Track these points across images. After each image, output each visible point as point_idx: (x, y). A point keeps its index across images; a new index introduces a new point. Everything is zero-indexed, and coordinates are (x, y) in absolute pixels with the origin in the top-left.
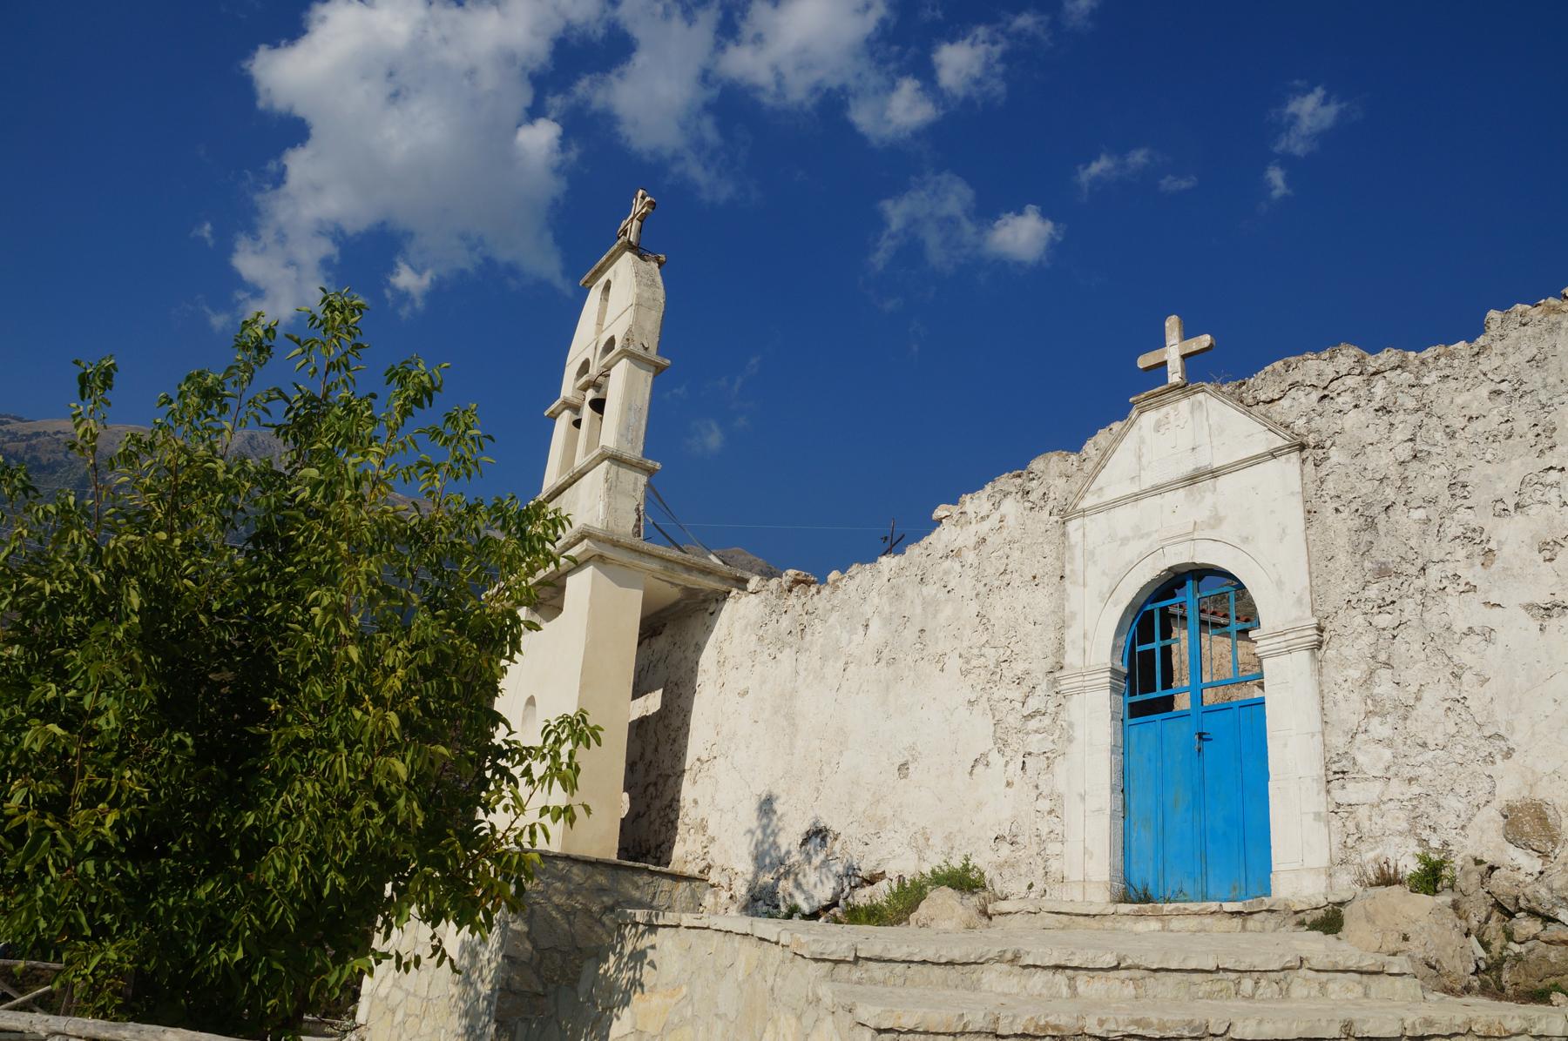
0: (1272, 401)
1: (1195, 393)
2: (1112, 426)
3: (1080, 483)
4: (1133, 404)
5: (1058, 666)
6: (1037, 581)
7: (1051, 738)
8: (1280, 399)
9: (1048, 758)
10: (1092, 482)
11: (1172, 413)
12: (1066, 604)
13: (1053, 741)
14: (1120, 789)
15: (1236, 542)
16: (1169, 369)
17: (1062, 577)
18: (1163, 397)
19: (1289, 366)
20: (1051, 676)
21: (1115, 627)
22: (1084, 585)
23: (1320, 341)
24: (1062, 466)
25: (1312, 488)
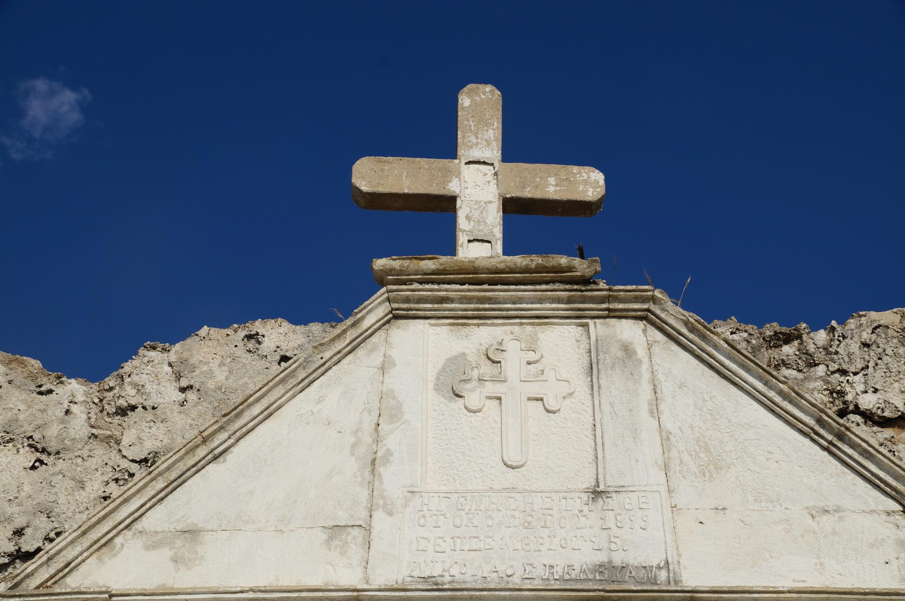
1: (612, 314)
2: (258, 326)
3: (95, 487)
4: (380, 281)
10: (160, 498)
16: (462, 223)
18: (500, 292)
23: (470, 83)
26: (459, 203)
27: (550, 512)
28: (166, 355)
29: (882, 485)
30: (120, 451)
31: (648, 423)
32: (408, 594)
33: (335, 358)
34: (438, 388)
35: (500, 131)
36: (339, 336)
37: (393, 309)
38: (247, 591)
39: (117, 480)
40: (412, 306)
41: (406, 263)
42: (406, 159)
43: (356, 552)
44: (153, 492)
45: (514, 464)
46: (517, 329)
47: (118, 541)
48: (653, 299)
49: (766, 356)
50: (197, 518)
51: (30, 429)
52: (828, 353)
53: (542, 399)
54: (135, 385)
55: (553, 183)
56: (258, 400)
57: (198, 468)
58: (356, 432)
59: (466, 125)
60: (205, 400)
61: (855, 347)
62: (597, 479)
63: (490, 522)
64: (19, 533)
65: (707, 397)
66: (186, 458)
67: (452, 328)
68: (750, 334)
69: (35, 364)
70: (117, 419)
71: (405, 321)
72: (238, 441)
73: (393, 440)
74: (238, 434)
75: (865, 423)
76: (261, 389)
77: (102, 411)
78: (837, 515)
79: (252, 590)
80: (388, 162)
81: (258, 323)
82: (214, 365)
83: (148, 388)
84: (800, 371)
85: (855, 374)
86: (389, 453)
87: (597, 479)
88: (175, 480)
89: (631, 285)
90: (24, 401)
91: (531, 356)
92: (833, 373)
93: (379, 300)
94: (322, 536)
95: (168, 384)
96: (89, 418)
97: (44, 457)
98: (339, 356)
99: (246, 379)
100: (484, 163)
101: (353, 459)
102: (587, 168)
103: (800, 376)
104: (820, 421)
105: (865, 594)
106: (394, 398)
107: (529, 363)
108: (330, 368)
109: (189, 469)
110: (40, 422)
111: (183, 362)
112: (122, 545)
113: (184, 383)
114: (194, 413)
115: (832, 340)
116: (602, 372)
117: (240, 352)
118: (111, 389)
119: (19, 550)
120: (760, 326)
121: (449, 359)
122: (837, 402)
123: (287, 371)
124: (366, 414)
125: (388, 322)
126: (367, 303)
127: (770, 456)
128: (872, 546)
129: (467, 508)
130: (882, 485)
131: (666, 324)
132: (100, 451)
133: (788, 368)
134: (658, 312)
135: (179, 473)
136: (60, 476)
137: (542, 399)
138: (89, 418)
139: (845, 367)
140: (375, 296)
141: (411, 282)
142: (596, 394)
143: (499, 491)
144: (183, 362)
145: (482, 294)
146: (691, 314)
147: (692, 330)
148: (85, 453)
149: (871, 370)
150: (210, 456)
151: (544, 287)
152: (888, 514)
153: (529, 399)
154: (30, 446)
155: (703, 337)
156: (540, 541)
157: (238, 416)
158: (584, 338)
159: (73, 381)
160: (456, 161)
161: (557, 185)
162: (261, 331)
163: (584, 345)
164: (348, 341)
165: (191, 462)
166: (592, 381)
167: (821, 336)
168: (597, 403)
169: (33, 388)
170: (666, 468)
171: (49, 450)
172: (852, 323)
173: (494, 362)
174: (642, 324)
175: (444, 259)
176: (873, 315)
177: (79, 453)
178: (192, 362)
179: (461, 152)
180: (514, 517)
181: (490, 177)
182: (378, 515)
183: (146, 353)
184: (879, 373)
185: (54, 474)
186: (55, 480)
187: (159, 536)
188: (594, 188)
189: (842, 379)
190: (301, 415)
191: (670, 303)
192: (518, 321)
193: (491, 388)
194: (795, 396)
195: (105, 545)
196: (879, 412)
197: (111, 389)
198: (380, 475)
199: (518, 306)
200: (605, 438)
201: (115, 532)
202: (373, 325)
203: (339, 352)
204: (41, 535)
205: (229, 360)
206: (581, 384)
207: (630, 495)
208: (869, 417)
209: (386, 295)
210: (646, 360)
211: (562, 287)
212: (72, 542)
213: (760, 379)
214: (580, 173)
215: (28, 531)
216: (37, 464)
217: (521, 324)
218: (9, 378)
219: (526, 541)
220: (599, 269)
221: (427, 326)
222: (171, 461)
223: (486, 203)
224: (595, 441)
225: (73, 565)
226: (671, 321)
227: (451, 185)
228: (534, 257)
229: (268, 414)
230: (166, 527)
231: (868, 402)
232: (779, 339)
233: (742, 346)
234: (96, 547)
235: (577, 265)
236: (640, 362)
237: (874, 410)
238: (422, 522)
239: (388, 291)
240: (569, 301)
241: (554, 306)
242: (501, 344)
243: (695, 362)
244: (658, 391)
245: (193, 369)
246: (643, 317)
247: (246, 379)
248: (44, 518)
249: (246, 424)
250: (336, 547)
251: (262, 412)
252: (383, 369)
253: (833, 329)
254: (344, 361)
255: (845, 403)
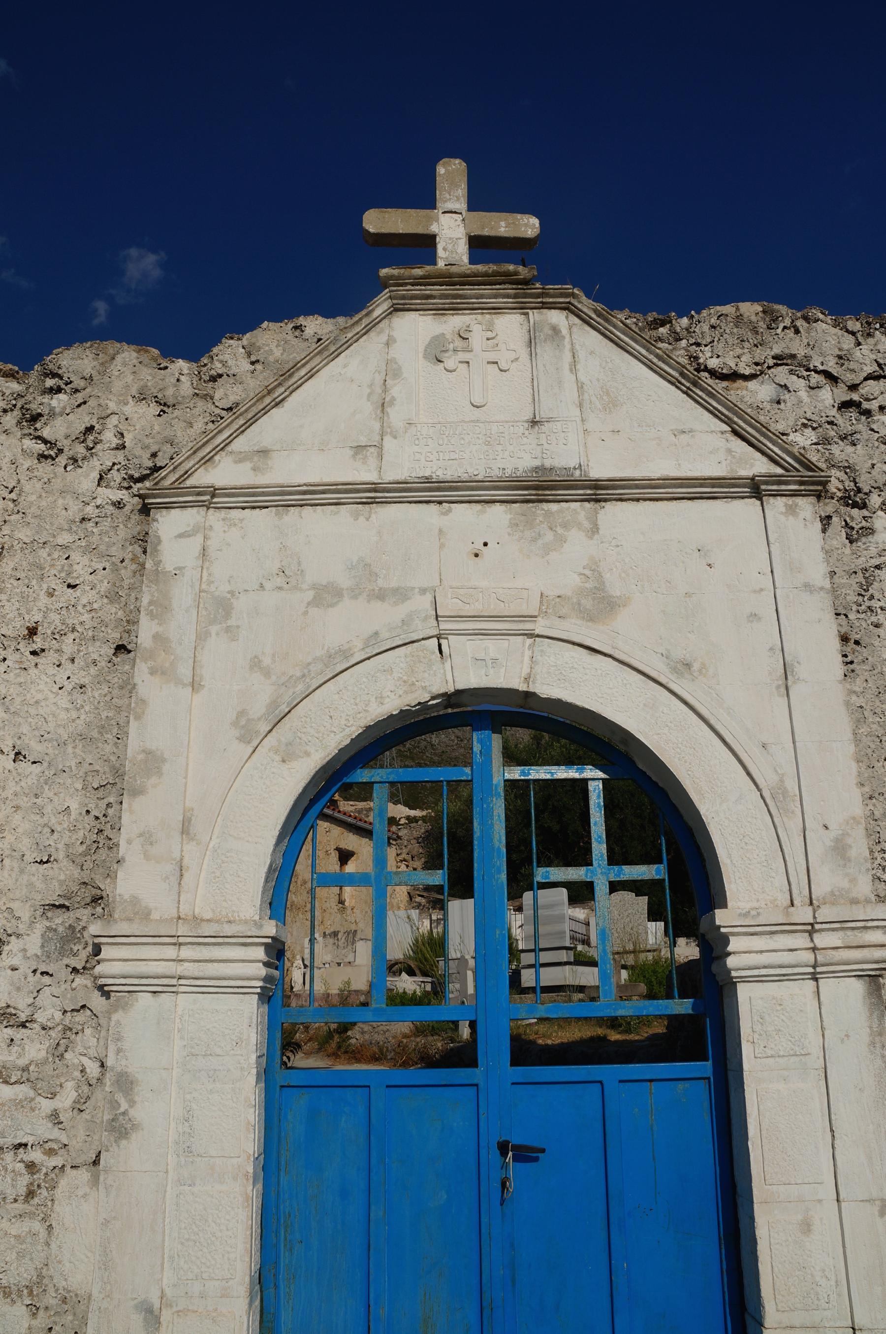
0: (734, 376)
1: (545, 306)
2: (301, 320)
3: (199, 426)
4: (384, 284)
5: (87, 894)
6: (38, 642)
7: (46, 1106)
8: (753, 377)
9: (31, 1167)
11: (477, 337)
12: (133, 726)
13: (55, 1118)
14: (269, 901)
15: (658, 669)
17: (121, 649)
18: (468, 290)
19: (775, 320)
20: (60, 920)
21: (282, 819)
22: (195, 685)
24: (149, 376)
25: (850, 588)
26: (438, 239)
27: (503, 435)
28: (240, 342)
29: (719, 415)
30: (214, 403)
31: (569, 378)
32: (408, 485)
33: (355, 338)
34: (426, 357)
35: (466, 190)
36: (357, 322)
37: (394, 304)
38: (302, 486)
39: (213, 422)
40: (407, 301)
41: (402, 271)
42: (400, 210)
43: (372, 462)
44: (237, 427)
45: (479, 405)
46: (479, 317)
47: (217, 458)
48: (573, 295)
49: (647, 334)
50: (266, 443)
51: (155, 391)
52: (689, 332)
53: (497, 363)
54: (221, 362)
55: (504, 225)
56: (304, 365)
57: (265, 411)
58: (371, 386)
59: (442, 187)
60: (268, 369)
61: (706, 328)
62: (534, 413)
63: (462, 442)
64: (154, 455)
65: (608, 360)
66: (258, 404)
67: (435, 317)
68: (638, 319)
69: (155, 352)
70: (211, 384)
71: (402, 313)
72: (291, 393)
73: (396, 391)
74: (291, 388)
75: (711, 378)
76: (305, 357)
77: (200, 380)
78: (691, 434)
79: (305, 485)
80: (388, 212)
81: (301, 318)
82: (273, 346)
83: (230, 363)
84: (670, 344)
85: (706, 346)
86: (393, 399)
87: (534, 413)
88: (251, 418)
89: (558, 285)
90: (151, 375)
91: (489, 334)
92: (692, 345)
93: (384, 298)
94: (351, 452)
95: (242, 360)
96: (192, 384)
97: (165, 409)
98: (357, 336)
99: (295, 354)
100: (455, 212)
101: (369, 403)
102: (527, 216)
103: (670, 347)
104: (682, 374)
105: (705, 479)
106: (396, 363)
107: (488, 339)
108: (351, 345)
109: (259, 412)
110: (161, 387)
111: (252, 345)
112: (220, 461)
113: (253, 358)
114: (261, 377)
115: (691, 324)
116: (538, 344)
117: (290, 337)
118: (205, 365)
119: (155, 466)
120: (645, 314)
121: (433, 337)
122: (693, 364)
123: (323, 346)
124: (377, 374)
125: (391, 313)
126: (376, 299)
127: (650, 397)
128: (711, 452)
129: (447, 433)
130: (719, 415)
131: (582, 312)
132: (200, 403)
133: (662, 342)
134: (576, 304)
135: (254, 414)
136: (177, 420)
137: (497, 363)
138: (192, 384)
139: (699, 341)
140: (381, 295)
141: (406, 284)
142: (534, 359)
143: (469, 422)
144: (252, 345)
145: (456, 292)
146: (599, 304)
147: (599, 315)
148: (192, 406)
149: (715, 343)
150: (273, 403)
151: (498, 287)
152: (722, 433)
153: (488, 363)
154: (156, 402)
155: (607, 320)
156: (496, 453)
157: (291, 376)
158: (526, 322)
159: (180, 360)
160: (436, 211)
161: (506, 227)
162: (304, 323)
163: (526, 327)
164: (363, 326)
165: (261, 407)
166: (531, 350)
167: (685, 321)
168: (534, 365)
169: (155, 366)
170: (581, 406)
171: (168, 404)
172: (705, 313)
173: (464, 339)
174: (565, 313)
175: (428, 268)
176: (718, 308)
177: (188, 405)
178: (258, 344)
179: (438, 204)
180: (478, 438)
181: (459, 222)
182: (387, 439)
183: (227, 341)
184: (721, 345)
185: (173, 419)
186: (173, 422)
187: (243, 455)
188: (532, 229)
189: (697, 349)
190: (333, 376)
191: (584, 298)
192: (480, 311)
193: (462, 356)
194: (665, 358)
195: (208, 460)
196: (720, 370)
197: (205, 365)
198: (388, 413)
199: (480, 300)
200: (540, 387)
201: (214, 452)
202: (380, 315)
203: (358, 333)
204: (168, 456)
205: (283, 342)
206: (524, 353)
207: (556, 423)
208: (713, 373)
209: (389, 294)
210: (568, 336)
211: (510, 286)
212: (188, 458)
213: (644, 347)
214: (523, 219)
215: (160, 454)
216: (161, 413)
217: (483, 313)
218: (140, 360)
219: (487, 453)
220: (536, 273)
221: (418, 316)
222: (247, 406)
223: (457, 239)
224: (533, 390)
225: (189, 472)
226: (585, 310)
227: (432, 227)
228: (491, 265)
229: (311, 375)
230: (247, 449)
231: (713, 363)
232: (657, 324)
233: (633, 327)
234: (203, 462)
235: (521, 271)
236: (564, 337)
237: (717, 369)
238: (417, 442)
239: (390, 291)
240: (515, 296)
241: (505, 300)
242: (469, 327)
243: (600, 337)
244: (576, 357)
245: (259, 349)
246: (567, 308)
247: (295, 354)
248: (169, 446)
249: (296, 382)
250: (360, 459)
251: (307, 374)
252: (388, 344)
253: (692, 317)
254: (361, 340)
255: (698, 364)
